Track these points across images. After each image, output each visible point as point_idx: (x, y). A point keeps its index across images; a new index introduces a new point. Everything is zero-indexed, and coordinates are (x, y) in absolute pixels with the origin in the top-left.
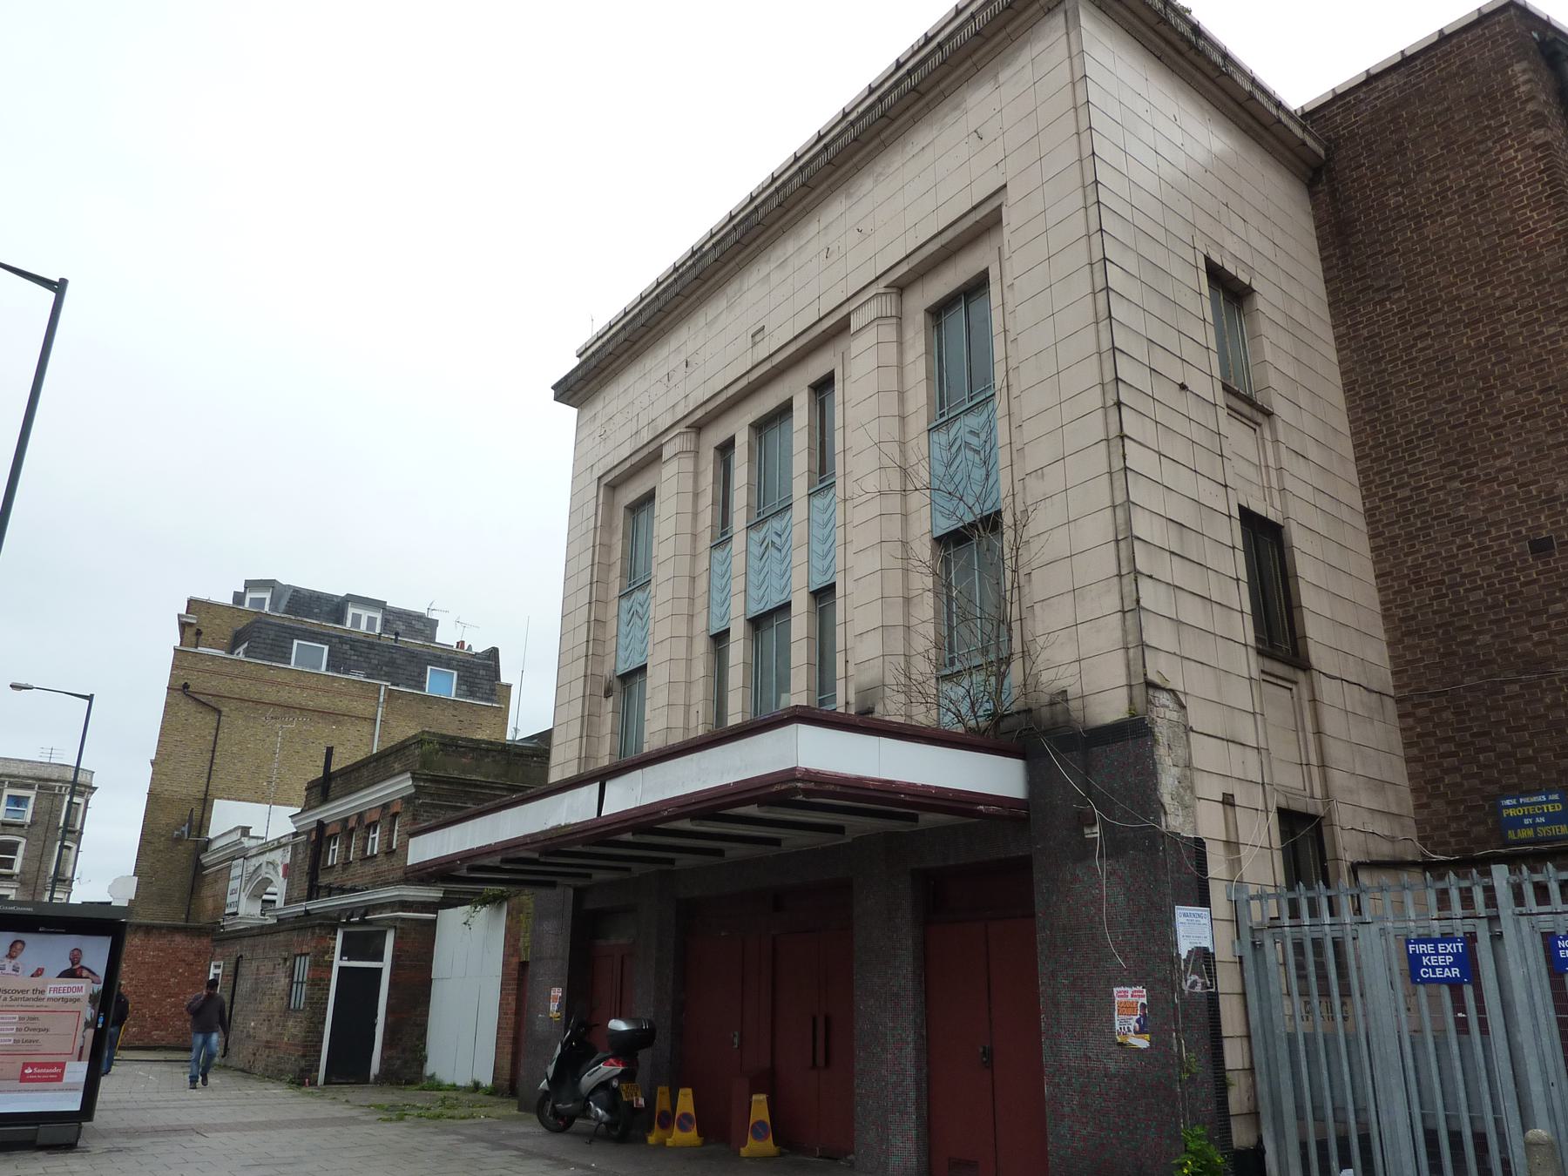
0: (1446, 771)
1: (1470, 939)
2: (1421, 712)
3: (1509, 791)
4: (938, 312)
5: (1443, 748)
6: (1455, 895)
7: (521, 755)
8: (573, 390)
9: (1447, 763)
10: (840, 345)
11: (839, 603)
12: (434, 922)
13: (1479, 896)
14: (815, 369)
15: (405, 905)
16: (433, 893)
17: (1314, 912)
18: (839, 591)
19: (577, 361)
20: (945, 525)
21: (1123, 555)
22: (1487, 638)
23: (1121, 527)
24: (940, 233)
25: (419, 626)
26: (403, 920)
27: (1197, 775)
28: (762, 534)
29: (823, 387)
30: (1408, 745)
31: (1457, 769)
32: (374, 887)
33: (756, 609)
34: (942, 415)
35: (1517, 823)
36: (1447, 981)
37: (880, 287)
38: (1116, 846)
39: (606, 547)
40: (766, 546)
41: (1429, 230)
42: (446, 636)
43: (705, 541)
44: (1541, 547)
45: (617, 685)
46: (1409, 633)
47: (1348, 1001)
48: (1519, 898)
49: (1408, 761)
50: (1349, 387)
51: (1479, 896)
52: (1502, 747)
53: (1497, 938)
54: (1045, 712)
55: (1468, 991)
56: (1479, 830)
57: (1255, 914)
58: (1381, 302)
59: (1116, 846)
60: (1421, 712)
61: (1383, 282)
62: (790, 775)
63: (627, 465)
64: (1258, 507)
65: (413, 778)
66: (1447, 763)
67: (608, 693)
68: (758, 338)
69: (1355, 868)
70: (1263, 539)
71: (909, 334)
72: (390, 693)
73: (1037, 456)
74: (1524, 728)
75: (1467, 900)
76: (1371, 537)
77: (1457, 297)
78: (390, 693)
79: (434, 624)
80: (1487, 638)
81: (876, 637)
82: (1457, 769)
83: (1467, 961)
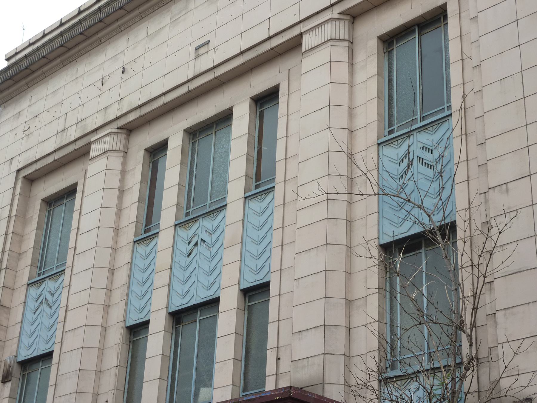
4: (390, 41)
10: (289, 63)
11: (273, 303)
14: (260, 83)
18: (274, 290)
19: (5, 64)
24: (36, 161)
27: (89, 121)
28: (191, 232)
29: (266, 99)
33: (178, 304)
34: (391, 132)
37: (335, 12)
39: (19, 237)
40: (195, 244)
43: (129, 235)
45: (16, 371)
63: (50, 159)
68: (202, 51)
71: (360, 57)
81: (319, 334)
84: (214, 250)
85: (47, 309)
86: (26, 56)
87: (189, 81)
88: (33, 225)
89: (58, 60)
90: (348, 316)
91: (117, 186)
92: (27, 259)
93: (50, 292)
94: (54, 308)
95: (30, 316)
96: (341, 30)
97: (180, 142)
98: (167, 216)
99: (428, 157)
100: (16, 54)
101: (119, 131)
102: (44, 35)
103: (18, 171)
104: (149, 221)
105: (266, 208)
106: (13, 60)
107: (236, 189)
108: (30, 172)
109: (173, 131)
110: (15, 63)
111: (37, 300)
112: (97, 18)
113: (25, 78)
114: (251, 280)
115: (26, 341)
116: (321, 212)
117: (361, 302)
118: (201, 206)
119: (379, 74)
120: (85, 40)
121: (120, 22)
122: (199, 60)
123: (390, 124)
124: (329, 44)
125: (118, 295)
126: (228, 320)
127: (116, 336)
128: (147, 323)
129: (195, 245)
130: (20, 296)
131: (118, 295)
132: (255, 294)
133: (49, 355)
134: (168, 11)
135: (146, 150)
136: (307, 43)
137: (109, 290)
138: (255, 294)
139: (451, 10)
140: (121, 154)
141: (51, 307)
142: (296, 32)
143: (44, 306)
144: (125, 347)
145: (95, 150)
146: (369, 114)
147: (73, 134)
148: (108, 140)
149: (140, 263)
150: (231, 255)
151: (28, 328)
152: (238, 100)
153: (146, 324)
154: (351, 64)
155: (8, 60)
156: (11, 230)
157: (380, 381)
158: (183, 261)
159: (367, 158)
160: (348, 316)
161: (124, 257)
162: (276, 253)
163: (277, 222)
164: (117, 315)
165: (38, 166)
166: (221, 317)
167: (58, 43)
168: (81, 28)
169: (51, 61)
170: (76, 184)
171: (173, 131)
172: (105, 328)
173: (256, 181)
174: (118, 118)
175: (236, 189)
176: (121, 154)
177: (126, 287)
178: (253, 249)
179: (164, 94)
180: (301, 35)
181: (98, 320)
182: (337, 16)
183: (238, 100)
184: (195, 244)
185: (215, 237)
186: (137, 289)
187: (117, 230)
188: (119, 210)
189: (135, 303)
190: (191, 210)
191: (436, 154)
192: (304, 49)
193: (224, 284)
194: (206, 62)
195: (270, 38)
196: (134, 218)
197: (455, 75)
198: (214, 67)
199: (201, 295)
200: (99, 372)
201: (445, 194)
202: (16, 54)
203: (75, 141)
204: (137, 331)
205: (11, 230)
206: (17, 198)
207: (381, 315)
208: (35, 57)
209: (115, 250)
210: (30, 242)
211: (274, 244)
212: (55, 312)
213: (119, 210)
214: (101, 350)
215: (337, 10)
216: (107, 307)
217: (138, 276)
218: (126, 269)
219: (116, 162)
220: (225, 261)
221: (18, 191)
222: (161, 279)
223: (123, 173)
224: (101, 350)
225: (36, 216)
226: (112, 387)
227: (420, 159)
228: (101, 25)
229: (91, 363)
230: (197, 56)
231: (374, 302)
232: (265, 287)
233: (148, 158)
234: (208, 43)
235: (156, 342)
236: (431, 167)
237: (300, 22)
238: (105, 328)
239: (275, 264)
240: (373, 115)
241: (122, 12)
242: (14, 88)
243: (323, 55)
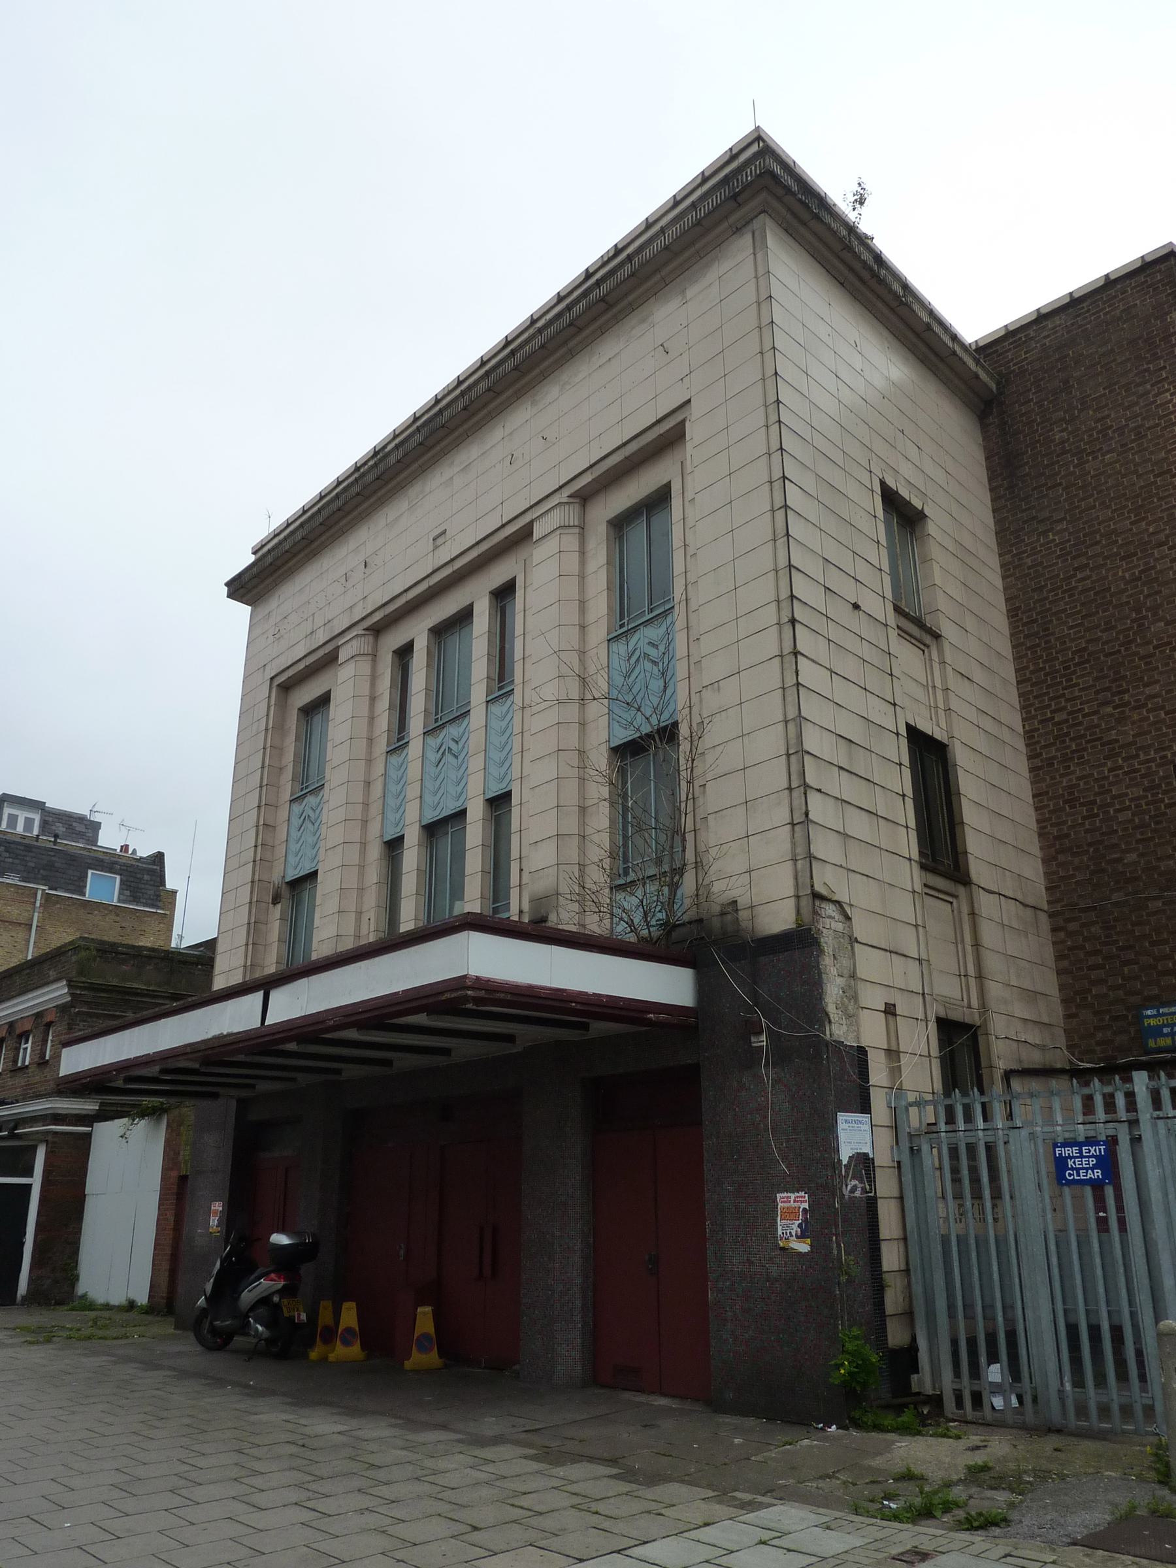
1: (1112, 1142)
2: (1072, 926)
4: (620, 524)
5: (1092, 961)
6: (1098, 1100)
7: (185, 963)
8: (243, 587)
9: (1094, 975)
10: (522, 553)
11: (515, 811)
12: (89, 1136)
13: (1120, 1101)
14: (497, 576)
15: (57, 1118)
16: (89, 1106)
17: (968, 1118)
18: (515, 800)
19: (252, 558)
20: (623, 735)
21: (794, 768)
22: (1133, 857)
23: (793, 741)
24: (288, 668)
25: (80, 828)
26: (56, 1133)
29: (504, 594)
30: (1059, 958)
32: (24, 1100)
33: (431, 816)
34: (622, 626)
35: (1157, 1032)
36: (1090, 1182)
37: (563, 497)
38: (782, 1054)
40: (444, 752)
42: (109, 839)
43: (381, 746)
46: (1062, 851)
48: (1157, 1103)
49: (1059, 972)
51: (1120, 1101)
53: (1136, 1141)
54: (716, 923)
55: (1109, 1191)
57: (914, 1119)
58: (1045, 533)
59: (782, 1054)
60: (1072, 926)
62: (460, 983)
63: (301, 666)
64: (925, 726)
65: (69, 986)
66: (1094, 975)
67: (276, 900)
68: (440, 541)
69: (1008, 1075)
72: (47, 897)
73: (715, 668)
75: (1110, 1106)
76: (1030, 758)
78: (47, 897)
79: (96, 826)
80: (1133, 857)
81: (551, 846)
83: (1109, 1163)
84: (461, 758)
85: (310, 826)
86: (269, 551)
87: (428, 576)
88: (292, 737)
89: (302, 555)
90: (583, 823)
91: (367, 693)
92: (288, 774)
93: (453, 740)
94: (316, 825)
95: (294, 834)
96: (571, 515)
97: (426, 643)
98: (416, 724)
99: (653, 652)
100: (263, 546)
101: (571, 500)
102: (288, 525)
103: (272, 679)
104: (501, 678)
105: (508, 712)
106: (260, 554)
107: (478, 694)
108: (668, 427)
109: (418, 631)
110: (264, 556)
112: (334, 507)
113: (271, 574)
114: (495, 790)
115: (292, 860)
116: (552, 717)
117: (594, 808)
118: (447, 714)
119: (609, 563)
120: (494, 398)
121: (360, 509)
123: (622, 618)
124: (558, 532)
125: (375, 808)
126: (475, 832)
127: (375, 852)
128: (402, 838)
129: (443, 754)
130: (283, 814)
131: (375, 808)
132: (499, 803)
133: (313, 875)
134: (643, 321)
135: (491, 593)
136: (538, 532)
137: (366, 805)
138: (499, 803)
139: (676, 488)
140: (370, 658)
141: (456, 757)
143: (308, 824)
144: (384, 863)
145: (343, 655)
146: (600, 607)
147: (321, 637)
148: (354, 642)
149: (393, 774)
150: (476, 763)
151: (294, 847)
152: (477, 595)
153: (401, 838)
154: (582, 552)
155: (254, 553)
156: (268, 745)
157: (611, 888)
158: (432, 770)
159: (598, 654)
160: (583, 823)
161: (379, 768)
162: (517, 759)
164: (374, 829)
165: (290, 673)
166: (470, 830)
167: (299, 535)
168: (320, 519)
169: (295, 555)
170: (668, 486)
171: (418, 631)
172: (364, 845)
173: (500, 682)
174: (363, 619)
175: (478, 694)
176: (370, 658)
177: (381, 801)
178: (496, 756)
179: (406, 591)
180: (531, 523)
181: (356, 836)
182: (565, 500)
183: (477, 595)
184: (444, 752)
185: (461, 744)
186: (391, 802)
187: (370, 740)
188: (372, 719)
189: (391, 817)
190: (625, 621)
191: (662, 648)
192: (536, 536)
193: (470, 794)
194: (445, 555)
195: (503, 526)
196: (385, 727)
197: (678, 566)
198: (452, 560)
199: (450, 808)
200: (361, 890)
201: (669, 692)
202: (263, 546)
203: (324, 644)
204: (394, 846)
205: (268, 745)
206: (272, 708)
207: (612, 822)
208: (278, 552)
209: (369, 761)
210: (289, 757)
211: (514, 751)
212: (463, 762)
213: (372, 719)
214: (362, 867)
215: (567, 492)
216: (365, 822)
217: (393, 788)
218: (381, 780)
219: (365, 667)
220: (470, 770)
221: (273, 702)
222: (413, 791)
223: (374, 678)
224: (362, 867)
225: (294, 727)
226: (373, 905)
227: (646, 655)
228: (340, 513)
229: (353, 882)
230: (436, 548)
231: (605, 808)
232: (506, 797)
233: (397, 660)
234: (444, 532)
235: (411, 858)
236: (655, 663)
237: (531, 507)
238: (364, 845)
239: (516, 773)
240: (603, 610)
241: (360, 498)
242: (328, 534)
243: (552, 545)
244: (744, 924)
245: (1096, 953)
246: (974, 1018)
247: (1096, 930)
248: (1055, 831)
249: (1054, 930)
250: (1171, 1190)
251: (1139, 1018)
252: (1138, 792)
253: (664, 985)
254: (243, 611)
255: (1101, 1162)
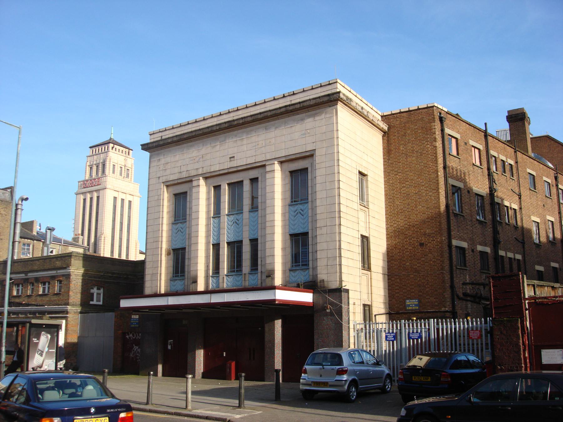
0: (396, 293)
3: (409, 298)
5: (396, 288)
14: (253, 174)
22: (408, 264)
27: (190, 172)
29: (254, 181)
31: (398, 293)
35: (409, 306)
41: (409, 159)
44: (422, 245)
46: (392, 260)
47: (330, 384)
50: (386, 195)
52: (408, 289)
56: (401, 307)
57: (359, 327)
60: (393, 279)
61: (396, 170)
64: (364, 234)
68: (232, 159)
69: (375, 316)
70: (365, 240)
74: (412, 285)
77: (412, 179)
80: (408, 264)
82: (398, 293)
111: (114, 165)
122: (231, 162)
142: (264, 163)
163: (260, 222)
185: (305, 212)
227: (300, 213)
232: (256, 240)
234: (234, 157)
244: (325, 285)
245: (397, 286)
246: (369, 303)
247: (398, 280)
248: (391, 255)
249: (388, 279)
250: (561, 196)
251: (405, 302)
252: (410, 248)
253: (307, 297)
254: (147, 154)
255: (394, 337)
